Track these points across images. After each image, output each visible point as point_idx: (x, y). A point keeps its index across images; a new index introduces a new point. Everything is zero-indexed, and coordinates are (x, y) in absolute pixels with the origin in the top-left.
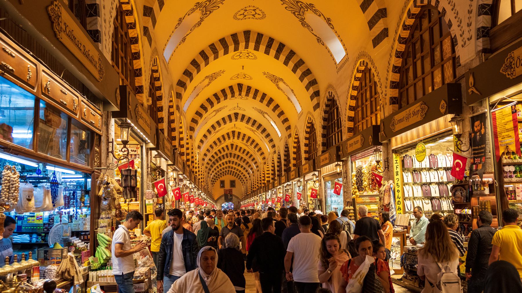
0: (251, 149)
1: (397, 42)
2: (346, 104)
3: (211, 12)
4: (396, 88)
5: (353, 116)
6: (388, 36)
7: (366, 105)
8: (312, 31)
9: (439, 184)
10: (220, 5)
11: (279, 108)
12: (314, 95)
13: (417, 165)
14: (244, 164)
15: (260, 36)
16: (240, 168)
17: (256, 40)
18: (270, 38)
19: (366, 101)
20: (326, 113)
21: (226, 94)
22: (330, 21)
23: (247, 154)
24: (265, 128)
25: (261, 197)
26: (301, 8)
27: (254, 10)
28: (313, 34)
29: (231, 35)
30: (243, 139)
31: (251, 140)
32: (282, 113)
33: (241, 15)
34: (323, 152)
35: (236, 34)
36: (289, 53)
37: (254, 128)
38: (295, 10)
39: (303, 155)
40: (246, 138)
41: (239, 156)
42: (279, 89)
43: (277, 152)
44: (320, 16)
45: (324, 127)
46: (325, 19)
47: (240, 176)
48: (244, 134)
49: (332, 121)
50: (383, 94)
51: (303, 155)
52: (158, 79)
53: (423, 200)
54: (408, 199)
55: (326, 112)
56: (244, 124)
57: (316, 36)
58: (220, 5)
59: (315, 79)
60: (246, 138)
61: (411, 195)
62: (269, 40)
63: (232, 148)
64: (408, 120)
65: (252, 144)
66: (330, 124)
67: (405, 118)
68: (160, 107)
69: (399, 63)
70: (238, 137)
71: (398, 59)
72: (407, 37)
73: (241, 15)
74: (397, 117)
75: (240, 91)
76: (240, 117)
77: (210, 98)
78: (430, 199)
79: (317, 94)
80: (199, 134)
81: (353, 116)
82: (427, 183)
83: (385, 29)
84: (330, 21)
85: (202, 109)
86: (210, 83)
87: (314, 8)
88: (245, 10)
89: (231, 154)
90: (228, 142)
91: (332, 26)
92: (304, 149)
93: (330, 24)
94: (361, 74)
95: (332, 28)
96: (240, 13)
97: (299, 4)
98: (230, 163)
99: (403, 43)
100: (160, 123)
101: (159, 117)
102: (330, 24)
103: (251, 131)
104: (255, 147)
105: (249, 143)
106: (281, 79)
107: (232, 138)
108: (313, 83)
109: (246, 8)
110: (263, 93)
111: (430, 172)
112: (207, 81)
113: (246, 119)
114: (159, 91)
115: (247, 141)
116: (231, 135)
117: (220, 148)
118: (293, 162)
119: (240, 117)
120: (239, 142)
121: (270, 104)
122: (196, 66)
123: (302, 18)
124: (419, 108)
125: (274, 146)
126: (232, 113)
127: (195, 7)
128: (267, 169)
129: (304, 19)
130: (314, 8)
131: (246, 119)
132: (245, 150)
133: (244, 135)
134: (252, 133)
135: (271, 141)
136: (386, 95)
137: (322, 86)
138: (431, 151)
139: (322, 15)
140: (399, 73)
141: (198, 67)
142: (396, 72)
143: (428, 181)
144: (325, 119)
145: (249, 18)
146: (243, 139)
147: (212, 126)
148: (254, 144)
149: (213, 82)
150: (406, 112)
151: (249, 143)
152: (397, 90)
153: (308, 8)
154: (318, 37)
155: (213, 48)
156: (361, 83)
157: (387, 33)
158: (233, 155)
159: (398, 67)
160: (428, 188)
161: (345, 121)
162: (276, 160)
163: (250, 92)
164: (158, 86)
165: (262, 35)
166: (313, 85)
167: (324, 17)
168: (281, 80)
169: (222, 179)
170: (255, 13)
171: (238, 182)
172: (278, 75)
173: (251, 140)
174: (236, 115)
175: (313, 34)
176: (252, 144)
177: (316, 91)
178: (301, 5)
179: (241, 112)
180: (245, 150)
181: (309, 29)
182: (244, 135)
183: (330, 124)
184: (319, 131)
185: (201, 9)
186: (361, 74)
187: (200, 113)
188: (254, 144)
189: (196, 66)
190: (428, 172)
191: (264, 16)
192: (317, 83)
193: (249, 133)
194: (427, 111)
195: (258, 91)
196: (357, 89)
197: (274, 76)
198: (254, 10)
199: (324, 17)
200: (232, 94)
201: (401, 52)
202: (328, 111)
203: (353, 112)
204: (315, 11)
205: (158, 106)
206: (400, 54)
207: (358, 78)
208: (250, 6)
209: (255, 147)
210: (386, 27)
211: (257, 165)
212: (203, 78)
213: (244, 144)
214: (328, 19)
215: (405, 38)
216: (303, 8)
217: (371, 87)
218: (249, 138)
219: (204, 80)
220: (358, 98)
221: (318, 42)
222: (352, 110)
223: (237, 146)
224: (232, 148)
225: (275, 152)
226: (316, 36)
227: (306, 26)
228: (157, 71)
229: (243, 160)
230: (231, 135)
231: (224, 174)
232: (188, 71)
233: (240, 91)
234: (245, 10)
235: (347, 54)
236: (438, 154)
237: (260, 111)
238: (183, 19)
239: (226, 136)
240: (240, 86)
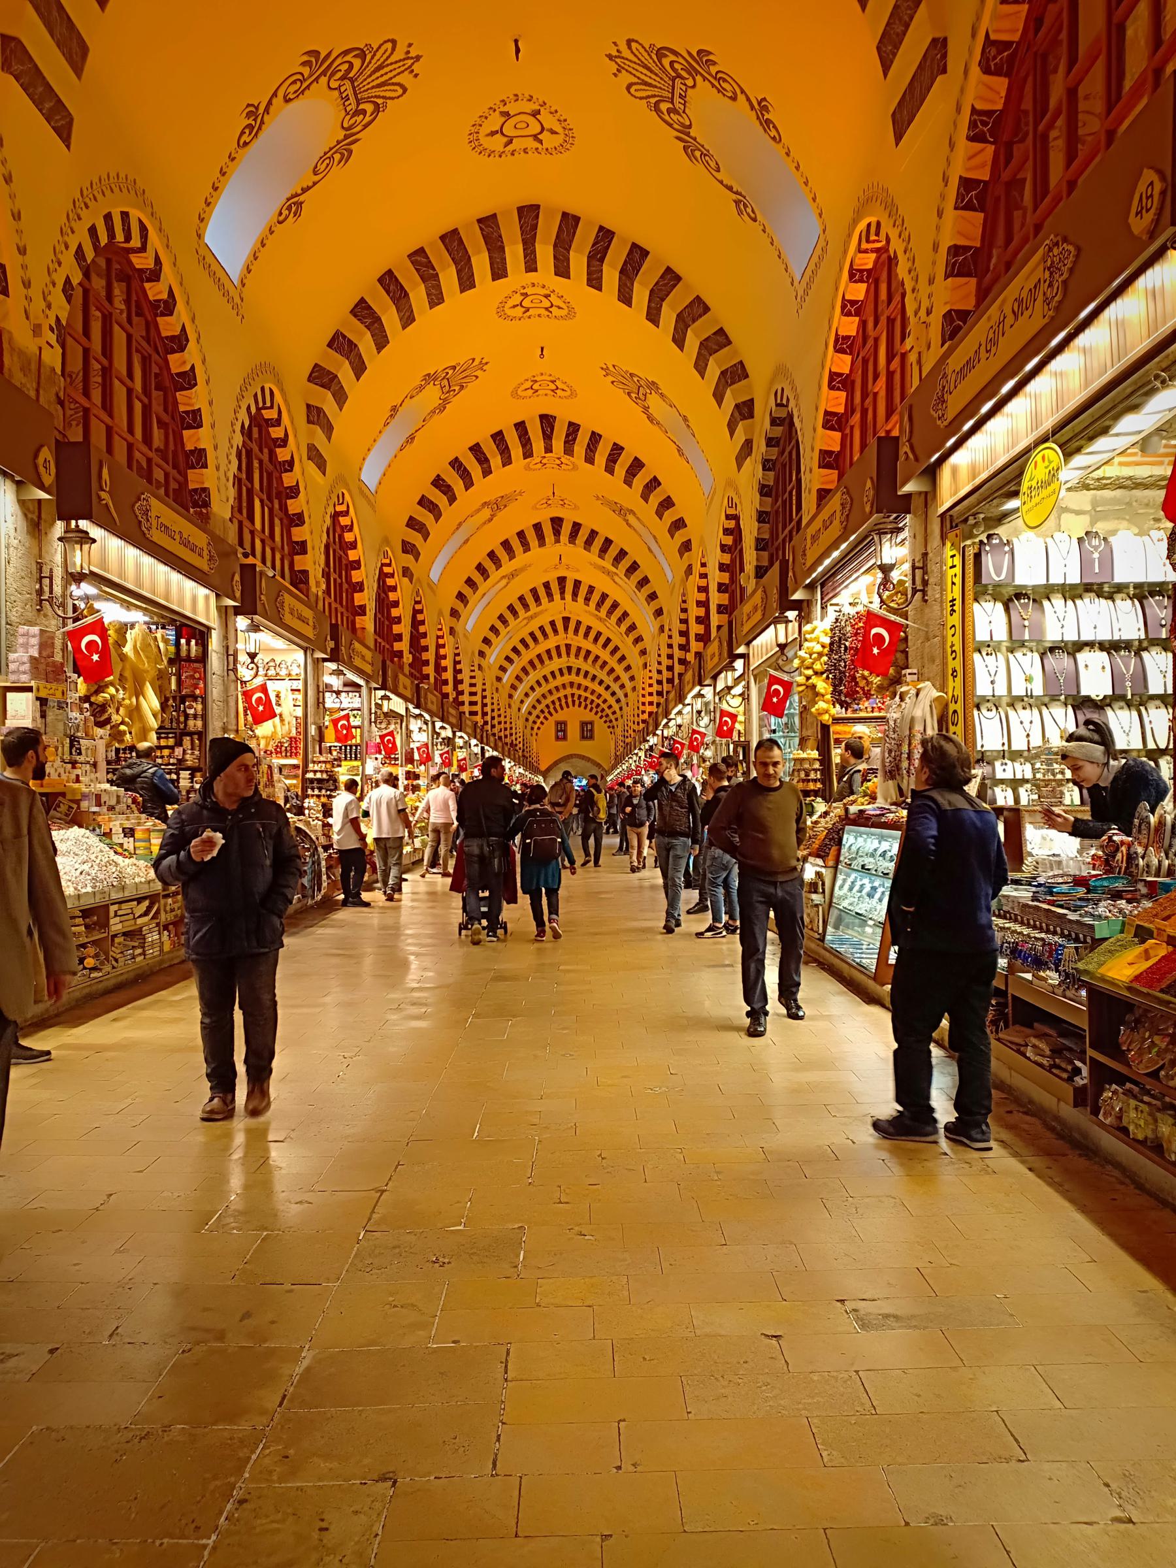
0: (611, 629)
1: (975, 70)
2: (817, 409)
3: (462, 387)
4: (969, 275)
5: (837, 448)
6: (944, 71)
7: (875, 394)
8: (718, 170)
9: (1111, 647)
10: (478, 373)
11: (658, 489)
12: (737, 414)
13: (1028, 575)
14: (602, 675)
15: (573, 429)
16: (594, 686)
17: (558, 237)
18: (601, 228)
19: (888, 416)
20: (769, 470)
21: (507, 447)
22: (768, 112)
23: (605, 646)
24: (635, 562)
25: (445, 382)
26: (673, 80)
27: (553, 382)
28: (721, 182)
29: (479, 221)
30: (587, 600)
31: (608, 604)
32: (667, 503)
33: (514, 306)
34: (760, 572)
35: (495, 215)
36: (662, 277)
37: (607, 564)
38: (656, 92)
39: (750, 557)
40: (596, 597)
41: (588, 652)
42: (652, 422)
43: (666, 629)
44: (734, 98)
45: (762, 517)
46: (752, 108)
47: (580, 696)
48: (590, 586)
49: (784, 491)
50: (922, 313)
51: (750, 557)
52: (421, 612)
53: (1044, 710)
54: (989, 705)
55: (767, 465)
56: (578, 550)
57: (730, 188)
58: (478, 373)
59: (741, 363)
60: (596, 597)
61: (1001, 690)
62: (597, 236)
63: (566, 629)
64: (993, 350)
65: (610, 612)
66: (780, 502)
67: (983, 348)
68: (187, 412)
69: (983, 165)
70: (575, 595)
71: (979, 146)
72: (1016, 37)
73: (514, 306)
74: (955, 363)
75: (557, 533)
76: (566, 529)
77: (461, 459)
78: (1073, 707)
79: (745, 410)
80: (494, 656)
81: (837, 448)
82: (1066, 643)
83: (934, 41)
84: (768, 112)
85: (437, 491)
86: (493, 516)
87: (713, 70)
88: (522, 294)
89: (568, 647)
90: (553, 610)
91: (773, 133)
92: (717, 602)
93: (767, 124)
94: (865, 285)
95: (774, 138)
96: (511, 303)
97: (635, 379)
98: (570, 673)
99: (997, 72)
100: (193, 467)
101: (189, 447)
102: (768, 121)
103: (604, 576)
104: (620, 621)
105: (603, 613)
106: (653, 383)
107: (557, 596)
108: (736, 374)
109: (504, 103)
110: (615, 444)
111: (1078, 602)
112: (486, 513)
113: (583, 535)
114: (177, 355)
115: (599, 605)
116: (555, 587)
117: (546, 671)
118: (695, 646)
119: (566, 529)
120: (579, 610)
121: (634, 476)
122: (368, 321)
123: (682, 125)
124: (1040, 273)
125: (659, 612)
126: (552, 577)
127: (306, 71)
128: (647, 678)
129: (690, 126)
130: (713, 70)
131: (583, 535)
132: (599, 634)
133: (591, 589)
134: (608, 579)
135: (653, 599)
136: (929, 313)
137: (759, 388)
138: (1093, 523)
139: (743, 92)
140: (982, 209)
141: (373, 323)
142: (969, 207)
143: (1071, 636)
144: (764, 491)
145: (525, 151)
146: (587, 600)
147: (489, 555)
148: (618, 613)
149: (500, 514)
150: (989, 319)
151: (603, 613)
152: (973, 281)
153: (697, 72)
154: (737, 193)
155: (420, 264)
156: (863, 324)
157: (944, 56)
158: (573, 651)
159: (978, 182)
160: (1066, 661)
161: (811, 471)
162: (694, 596)
163: (574, 439)
164: (169, 334)
165: (577, 219)
166: (733, 383)
167: (748, 99)
168: (632, 512)
169: (560, 716)
170: (539, 129)
171: (600, 726)
172: (626, 505)
173: (608, 604)
174: (557, 522)
175: (721, 182)
176: (610, 612)
177: (744, 403)
178: (672, 63)
179: (569, 517)
180: (599, 634)
181: (707, 165)
182: (591, 589)
183: (780, 502)
184: (750, 530)
185: (334, 84)
186: (865, 285)
187: (432, 502)
188: (618, 613)
189: (368, 321)
190: (1070, 603)
191: (571, 313)
192: (747, 376)
193: (603, 584)
194: (1071, 270)
195: (600, 436)
196: (851, 347)
197: (632, 375)
198: (553, 382)
199: (748, 99)
200: (524, 446)
201: (989, 113)
202: (774, 462)
203: (837, 435)
204: (719, 81)
205: (182, 408)
206: (985, 124)
207: (853, 303)
208: (533, 285)
209: (620, 621)
210: (938, 35)
211: (630, 673)
212: (418, 382)
213: (600, 619)
214: (759, 104)
215: (1007, 45)
216: (679, 76)
217: (894, 320)
218: (604, 597)
219: (421, 388)
220: (853, 382)
221: (740, 213)
222: (832, 428)
223: (579, 623)
224: (566, 629)
225: (689, 570)
226: (730, 188)
227: (698, 154)
228: (421, 612)
229: (600, 662)
230: (555, 587)
231: (564, 703)
232: (344, 337)
233: (557, 533)
234: (522, 294)
235: (824, 231)
236: (1114, 532)
237: (615, 507)
238: (267, 110)
239: (542, 592)
240: (547, 421)
